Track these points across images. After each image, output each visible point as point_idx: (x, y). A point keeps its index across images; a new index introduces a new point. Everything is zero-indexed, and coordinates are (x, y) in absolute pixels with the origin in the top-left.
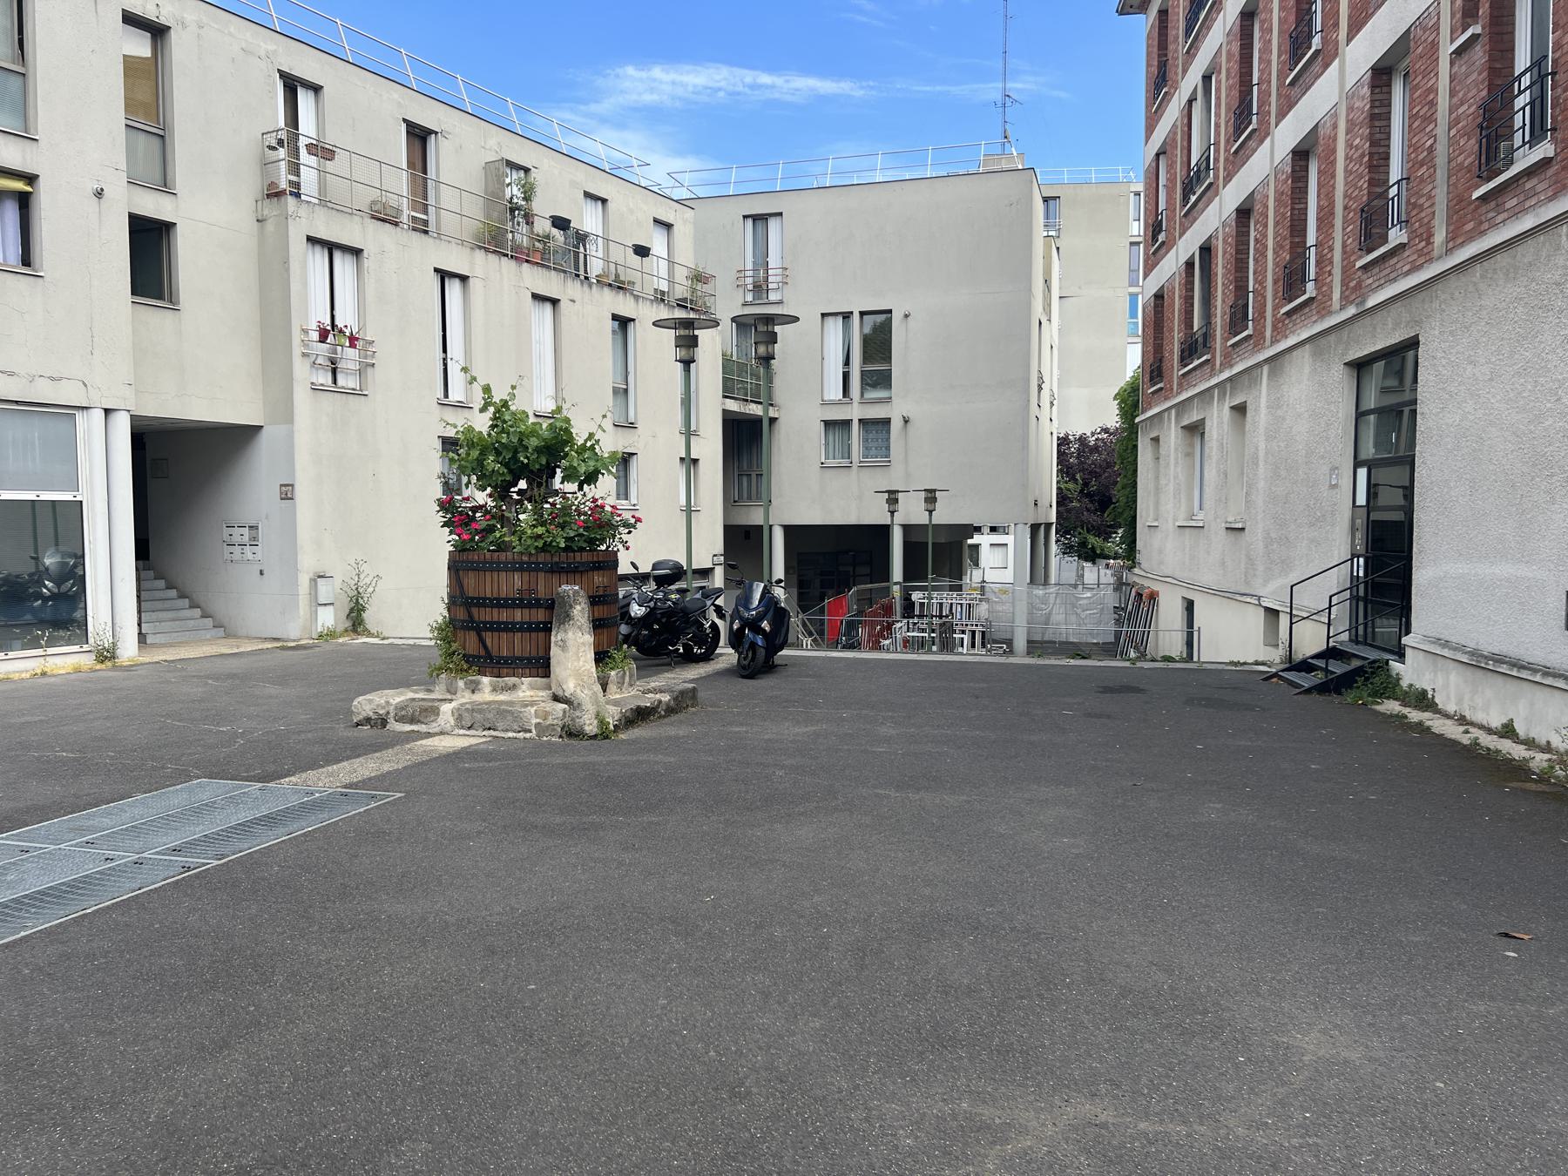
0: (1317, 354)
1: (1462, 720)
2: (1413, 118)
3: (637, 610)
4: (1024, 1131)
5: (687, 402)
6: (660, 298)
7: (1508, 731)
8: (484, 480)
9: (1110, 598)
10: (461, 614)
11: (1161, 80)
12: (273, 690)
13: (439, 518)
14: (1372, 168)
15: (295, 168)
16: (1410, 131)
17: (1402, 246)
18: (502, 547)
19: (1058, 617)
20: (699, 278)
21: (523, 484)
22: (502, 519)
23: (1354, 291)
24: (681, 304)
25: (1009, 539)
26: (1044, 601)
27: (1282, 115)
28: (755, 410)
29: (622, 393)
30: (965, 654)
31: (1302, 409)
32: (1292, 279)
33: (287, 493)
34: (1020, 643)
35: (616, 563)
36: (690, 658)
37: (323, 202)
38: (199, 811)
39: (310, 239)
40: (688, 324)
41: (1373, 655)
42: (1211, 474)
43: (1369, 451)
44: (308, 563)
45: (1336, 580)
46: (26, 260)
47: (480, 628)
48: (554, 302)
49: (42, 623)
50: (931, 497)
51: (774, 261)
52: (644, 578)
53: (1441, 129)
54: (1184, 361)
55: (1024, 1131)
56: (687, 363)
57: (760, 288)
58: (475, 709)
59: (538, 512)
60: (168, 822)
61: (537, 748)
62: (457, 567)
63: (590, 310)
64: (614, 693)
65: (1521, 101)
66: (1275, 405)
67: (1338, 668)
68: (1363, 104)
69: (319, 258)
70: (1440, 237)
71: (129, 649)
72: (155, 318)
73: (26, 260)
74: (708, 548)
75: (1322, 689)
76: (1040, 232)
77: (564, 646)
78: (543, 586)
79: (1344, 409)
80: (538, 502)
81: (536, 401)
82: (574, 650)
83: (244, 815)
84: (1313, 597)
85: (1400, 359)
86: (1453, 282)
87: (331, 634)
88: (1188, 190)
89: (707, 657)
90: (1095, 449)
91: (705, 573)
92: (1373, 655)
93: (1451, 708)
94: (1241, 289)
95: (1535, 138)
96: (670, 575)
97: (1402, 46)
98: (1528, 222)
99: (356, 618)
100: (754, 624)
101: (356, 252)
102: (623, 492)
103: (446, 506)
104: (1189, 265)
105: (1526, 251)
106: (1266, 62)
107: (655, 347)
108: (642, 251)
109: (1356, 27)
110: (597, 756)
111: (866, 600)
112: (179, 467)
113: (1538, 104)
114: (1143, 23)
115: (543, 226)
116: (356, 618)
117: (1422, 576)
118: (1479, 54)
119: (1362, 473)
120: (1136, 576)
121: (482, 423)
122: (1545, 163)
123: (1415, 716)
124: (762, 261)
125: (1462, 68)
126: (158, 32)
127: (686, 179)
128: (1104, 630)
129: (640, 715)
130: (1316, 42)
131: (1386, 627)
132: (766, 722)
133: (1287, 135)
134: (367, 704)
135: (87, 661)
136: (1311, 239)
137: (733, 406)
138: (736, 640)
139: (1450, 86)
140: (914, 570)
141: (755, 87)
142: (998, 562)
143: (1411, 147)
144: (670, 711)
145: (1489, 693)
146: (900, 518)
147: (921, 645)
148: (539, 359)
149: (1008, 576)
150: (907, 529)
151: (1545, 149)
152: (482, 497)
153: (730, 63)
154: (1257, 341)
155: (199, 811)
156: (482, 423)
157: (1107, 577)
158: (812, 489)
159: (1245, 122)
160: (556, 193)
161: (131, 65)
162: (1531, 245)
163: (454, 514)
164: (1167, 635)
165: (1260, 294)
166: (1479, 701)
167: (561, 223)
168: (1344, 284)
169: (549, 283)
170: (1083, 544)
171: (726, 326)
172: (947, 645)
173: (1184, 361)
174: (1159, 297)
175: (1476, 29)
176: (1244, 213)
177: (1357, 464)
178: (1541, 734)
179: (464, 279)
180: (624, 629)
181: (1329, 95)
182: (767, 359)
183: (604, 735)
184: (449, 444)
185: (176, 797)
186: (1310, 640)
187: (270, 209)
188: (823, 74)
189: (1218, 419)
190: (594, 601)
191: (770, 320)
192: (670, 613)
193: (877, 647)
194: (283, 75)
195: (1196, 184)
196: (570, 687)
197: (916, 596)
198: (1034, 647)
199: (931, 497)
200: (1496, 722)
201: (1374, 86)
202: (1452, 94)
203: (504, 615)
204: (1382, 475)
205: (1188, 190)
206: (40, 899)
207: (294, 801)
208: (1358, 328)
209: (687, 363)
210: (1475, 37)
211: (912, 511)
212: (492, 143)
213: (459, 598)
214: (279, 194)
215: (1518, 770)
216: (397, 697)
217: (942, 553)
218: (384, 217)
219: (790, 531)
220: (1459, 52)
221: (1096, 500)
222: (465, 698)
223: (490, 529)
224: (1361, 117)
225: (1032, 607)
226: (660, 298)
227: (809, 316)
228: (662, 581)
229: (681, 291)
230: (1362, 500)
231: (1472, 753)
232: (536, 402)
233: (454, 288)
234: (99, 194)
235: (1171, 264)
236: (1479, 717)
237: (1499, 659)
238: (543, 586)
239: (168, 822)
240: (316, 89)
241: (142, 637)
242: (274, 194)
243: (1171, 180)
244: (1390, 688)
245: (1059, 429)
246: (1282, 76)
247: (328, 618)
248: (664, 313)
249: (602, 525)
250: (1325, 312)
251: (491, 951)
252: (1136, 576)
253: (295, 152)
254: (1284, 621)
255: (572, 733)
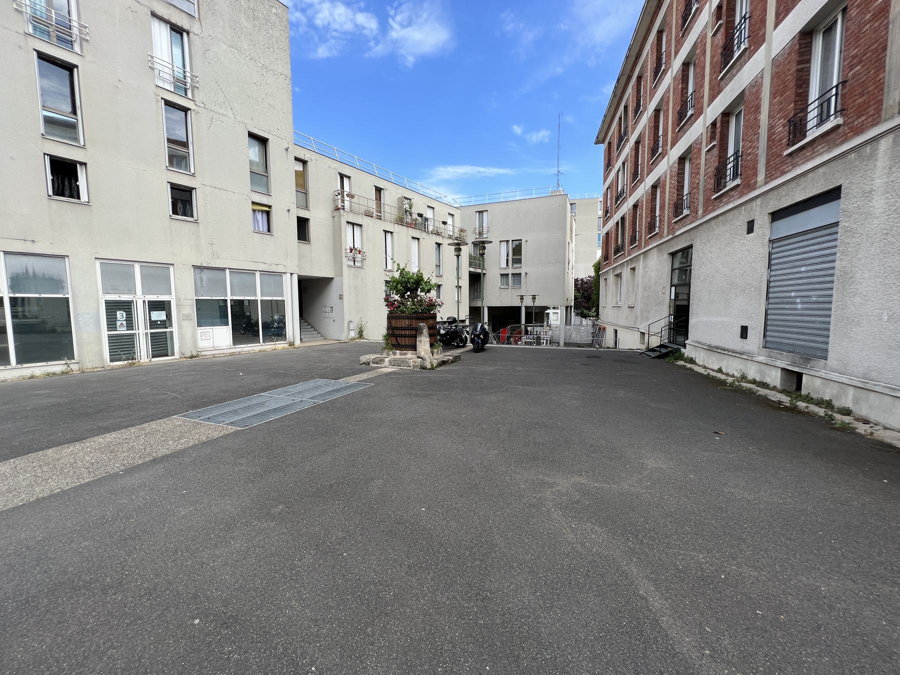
0: (659, 251)
1: (705, 367)
2: (692, 173)
3: (442, 332)
4: (558, 485)
5: (458, 269)
6: (450, 237)
7: (720, 371)
8: (397, 292)
9: (591, 330)
10: (391, 332)
11: (609, 165)
12: (337, 354)
13: (385, 304)
14: (678, 190)
15: (343, 201)
16: (691, 177)
17: (688, 215)
18: (402, 312)
19: (574, 335)
20: (462, 231)
21: (409, 293)
22: (403, 304)
23: (671, 230)
24: (457, 239)
25: (559, 311)
26: (569, 330)
27: (648, 174)
28: (479, 271)
29: (438, 266)
30: (543, 346)
31: (654, 268)
32: (651, 227)
33: (341, 297)
34: (562, 343)
35: (436, 317)
36: (458, 347)
37: (351, 211)
38: (317, 388)
39: (348, 222)
40: (458, 244)
41: (675, 346)
42: (624, 289)
43: (676, 281)
44: (347, 318)
45: (664, 323)
46: (269, 231)
47: (396, 336)
48: (418, 239)
49: (274, 335)
50: (534, 298)
51: (485, 225)
52: (445, 322)
53: (702, 177)
54: (615, 254)
55: (558, 485)
56: (458, 256)
57: (480, 234)
58: (395, 360)
59: (413, 301)
60: (309, 390)
61: (413, 372)
62: (390, 318)
63: (429, 241)
64: (436, 356)
65: (729, 166)
66: (645, 267)
67: (664, 351)
68: (675, 170)
69: (350, 227)
70: (700, 212)
71: (298, 343)
72: (304, 246)
73: (269, 231)
74: (464, 314)
75: (658, 357)
76: (569, 214)
77: (420, 342)
78: (414, 323)
79: (667, 268)
80: (413, 299)
81: (413, 269)
82: (424, 343)
83: (330, 389)
84: (656, 329)
85: (687, 251)
86: (705, 226)
87: (354, 339)
88: (617, 199)
89: (464, 346)
90: (586, 283)
91: (463, 321)
92: (675, 346)
93: (701, 363)
94: (634, 231)
95: (734, 178)
96: (453, 321)
97: (689, 150)
98: (731, 206)
99: (361, 334)
100: (478, 336)
101: (361, 226)
102: (438, 296)
103: (386, 300)
104: (617, 223)
105: (730, 216)
106: (643, 157)
107: (448, 251)
108: (445, 223)
109: (673, 144)
110: (431, 375)
111: (513, 330)
112: (311, 289)
113: (736, 167)
114: (603, 147)
115: (415, 216)
116: (361, 334)
117: (692, 321)
118: (715, 151)
119: (673, 288)
120: (599, 322)
121: (397, 275)
122: (738, 186)
123: (689, 366)
124: (481, 226)
125: (709, 156)
126: (304, 162)
127: (458, 201)
128: (588, 339)
129: (443, 363)
130: (660, 150)
131: (680, 339)
132: (481, 366)
133: (650, 181)
134: (364, 358)
135: (287, 346)
136: (657, 214)
137: (472, 270)
138: (472, 341)
139: (705, 162)
140: (528, 321)
141: (479, 172)
142: (555, 318)
143: (691, 183)
144: (452, 362)
145: (714, 358)
146: (524, 304)
147: (531, 344)
148: (413, 256)
149: (558, 323)
150: (526, 307)
151: (738, 181)
152: (397, 297)
153: (472, 165)
154: (639, 247)
155: (317, 388)
156: (397, 275)
157: (590, 323)
158: (496, 295)
159: (636, 176)
160: (419, 206)
161: (297, 173)
162: (731, 213)
163: (389, 303)
164: (608, 340)
165: (640, 232)
166: (710, 361)
167: (420, 215)
168: (668, 228)
169: (417, 233)
170: (582, 313)
171: (471, 246)
172: (539, 344)
173: (615, 254)
174: (607, 234)
175: (715, 143)
176: (635, 206)
177: (672, 286)
178: (731, 372)
179: (392, 233)
180: (438, 337)
181: (664, 167)
182: (482, 255)
183: (432, 368)
184: (387, 282)
185: (311, 384)
186: (655, 342)
187: (336, 214)
188: (500, 167)
189: (626, 272)
190: (430, 328)
191: (483, 242)
192: (453, 332)
193: (516, 344)
194: (340, 174)
195: (619, 198)
196: (423, 354)
197: (529, 328)
198: (566, 344)
199: (534, 298)
200: (716, 368)
201: (679, 164)
202: (706, 165)
203: (403, 332)
204: (681, 290)
205: (617, 199)
206: (276, 410)
207: (344, 385)
208: (673, 242)
209: (458, 256)
210: (714, 146)
211: (528, 302)
212: (400, 191)
213: (390, 327)
214: (338, 209)
215: (723, 383)
216: (372, 357)
217: (538, 315)
218: (368, 215)
219: (489, 308)
220: (708, 151)
221: (587, 298)
222: (392, 357)
223: (399, 307)
224: (674, 174)
225: (565, 332)
226: (450, 237)
227: (496, 242)
228: (450, 323)
229: (457, 235)
230: (673, 297)
231: (707, 377)
232: (413, 269)
233: (389, 235)
234: (289, 211)
235: (611, 223)
236: (710, 366)
237: (717, 348)
238: (414, 323)
239: (309, 390)
240: (349, 178)
241: (301, 339)
242: (337, 209)
243: (612, 197)
244: (681, 357)
245: (575, 276)
246: (648, 161)
247: (353, 334)
248: (451, 241)
249: (432, 305)
250: (662, 237)
251: (400, 428)
252: (599, 322)
253: (343, 197)
254: (647, 336)
255: (423, 368)
